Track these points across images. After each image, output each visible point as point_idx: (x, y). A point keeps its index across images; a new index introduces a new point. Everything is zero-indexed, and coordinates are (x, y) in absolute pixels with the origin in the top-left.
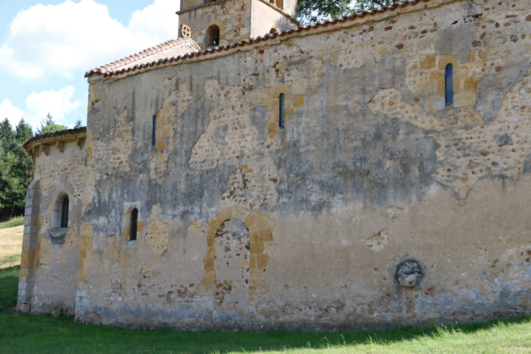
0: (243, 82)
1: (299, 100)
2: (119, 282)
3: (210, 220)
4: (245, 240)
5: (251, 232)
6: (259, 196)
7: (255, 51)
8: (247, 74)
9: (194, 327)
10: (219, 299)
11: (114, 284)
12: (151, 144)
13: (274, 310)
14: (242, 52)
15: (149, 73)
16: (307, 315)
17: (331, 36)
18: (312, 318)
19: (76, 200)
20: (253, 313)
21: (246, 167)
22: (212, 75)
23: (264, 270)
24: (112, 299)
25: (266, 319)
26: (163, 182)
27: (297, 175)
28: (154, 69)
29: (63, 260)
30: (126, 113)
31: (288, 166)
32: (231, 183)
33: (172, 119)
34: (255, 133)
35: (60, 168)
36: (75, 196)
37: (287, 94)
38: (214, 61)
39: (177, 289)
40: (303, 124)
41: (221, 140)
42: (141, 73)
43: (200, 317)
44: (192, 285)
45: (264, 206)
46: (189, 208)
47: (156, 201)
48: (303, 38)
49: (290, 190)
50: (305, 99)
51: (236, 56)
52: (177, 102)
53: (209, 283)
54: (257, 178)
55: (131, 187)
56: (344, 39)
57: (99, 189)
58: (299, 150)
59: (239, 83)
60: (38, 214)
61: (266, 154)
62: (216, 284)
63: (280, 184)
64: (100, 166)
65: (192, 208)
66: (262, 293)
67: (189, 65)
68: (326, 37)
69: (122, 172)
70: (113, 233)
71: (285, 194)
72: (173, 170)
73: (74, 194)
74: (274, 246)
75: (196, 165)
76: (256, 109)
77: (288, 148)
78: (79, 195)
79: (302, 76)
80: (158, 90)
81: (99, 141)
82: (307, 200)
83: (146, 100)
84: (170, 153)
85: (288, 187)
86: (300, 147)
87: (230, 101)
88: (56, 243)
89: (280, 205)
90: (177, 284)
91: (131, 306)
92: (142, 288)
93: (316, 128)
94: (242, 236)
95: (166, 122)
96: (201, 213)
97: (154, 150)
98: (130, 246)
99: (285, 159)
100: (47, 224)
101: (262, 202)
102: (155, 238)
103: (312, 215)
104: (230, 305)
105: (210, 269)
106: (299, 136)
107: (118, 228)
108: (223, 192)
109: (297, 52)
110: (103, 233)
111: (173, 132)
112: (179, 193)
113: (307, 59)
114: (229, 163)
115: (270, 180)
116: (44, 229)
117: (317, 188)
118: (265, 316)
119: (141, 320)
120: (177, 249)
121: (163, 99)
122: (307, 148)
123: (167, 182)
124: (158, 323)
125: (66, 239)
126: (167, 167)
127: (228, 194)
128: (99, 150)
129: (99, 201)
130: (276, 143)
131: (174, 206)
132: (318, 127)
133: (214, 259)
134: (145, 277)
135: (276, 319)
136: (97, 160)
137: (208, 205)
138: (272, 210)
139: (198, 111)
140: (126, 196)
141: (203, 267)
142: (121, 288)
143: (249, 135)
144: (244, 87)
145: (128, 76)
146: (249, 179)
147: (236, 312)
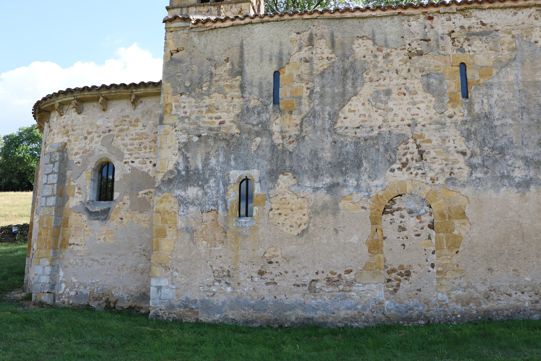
0: (408, 46)
1: (485, 71)
2: (226, 267)
3: (373, 194)
4: (427, 219)
5: (435, 209)
6: (443, 170)
7: (422, 17)
8: (414, 39)
9: (357, 322)
10: (392, 286)
11: (217, 270)
12: (272, 103)
13: (475, 296)
14: (404, 15)
15: (265, 25)
16: (518, 300)
17: (520, 12)
18: (527, 304)
19: (127, 167)
20: (444, 301)
21: (421, 136)
22: (363, 34)
23: (457, 252)
24: (214, 290)
25: (464, 308)
26: (296, 148)
27: (493, 149)
28: (273, 21)
29: (108, 240)
30: (228, 66)
31: (480, 139)
32: (402, 153)
33: (306, 77)
34: (431, 101)
35: (100, 129)
36: (125, 163)
37: (470, 64)
38: (365, 20)
39: (326, 276)
40: (495, 96)
41: (383, 105)
42: (254, 23)
43: (364, 309)
44: (349, 272)
45: (451, 180)
46: (340, 180)
47: (285, 170)
48: (484, 11)
49: (485, 165)
50: (495, 71)
51: (396, 18)
52: (311, 59)
53: (376, 268)
54: (438, 150)
55: (242, 152)
56: (537, 17)
57: (185, 153)
58: (492, 122)
59: (403, 47)
60: (65, 183)
61: (448, 124)
62: (387, 270)
63: (471, 157)
64: (186, 126)
65: (345, 181)
66: (456, 278)
67: (328, 21)
68: (513, 13)
69: (226, 135)
70: (212, 207)
71: (480, 168)
72: (310, 135)
73: (124, 161)
74: (469, 225)
75: (347, 130)
76: (430, 76)
77: (477, 119)
78: (133, 162)
79: (487, 47)
80: (281, 44)
81: (183, 96)
82: (508, 176)
83: (261, 54)
84: (303, 115)
85: (483, 161)
86: (494, 120)
87: (392, 64)
88: (96, 219)
89: (473, 181)
90: (325, 270)
91: (249, 298)
92: (265, 276)
93: (512, 102)
94: (423, 214)
95: (296, 80)
96: (358, 187)
97: (278, 111)
98: (244, 224)
99: (476, 131)
100: (80, 196)
101: (448, 176)
102: (286, 215)
103: (518, 192)
104: (410, 294)
105: (376, 252)
106: (491, 108)
107: (220, 202)
108: (394, 162)
109: (477, 24)
110: (195, 208)
111: (309, 91)
112: (322, 162)
113: (492, 32)
114: (396, 131)
115: (458, 152)
116: (74, 202)
117: (520, 163)
118: (462, 303)
119: (268, 315)
120: (324, 229)
121: (289, 54)
122: (503, 121)
123: (301, 148)
124: (296, 319)
125: (112, 214)
126: (301, 131)
127: (400, 166)
128: (184, 107)
129: (187, 169)
130: (461, 114)
131: (316, 178)
132: (514, 100)
133: (382, 241)
134: (271, 263)
135: (477, 307)
136: (182, 119)
137: (369, 177)
138: (464, 185)
139: (346, 71)
140: (233, 163)
141: (367, 250)
142: (229, 276)
143: (422, 102)
144: (410, 52)
145: (233, 25)
146: (427, 150)
147: (420, 302)
